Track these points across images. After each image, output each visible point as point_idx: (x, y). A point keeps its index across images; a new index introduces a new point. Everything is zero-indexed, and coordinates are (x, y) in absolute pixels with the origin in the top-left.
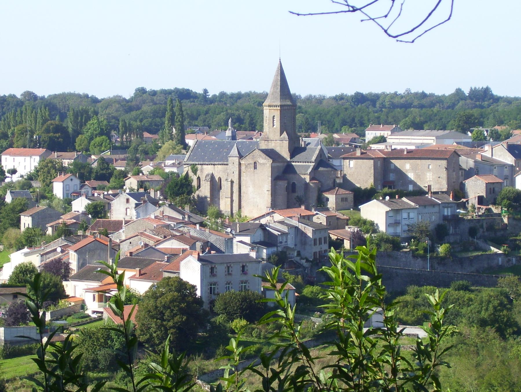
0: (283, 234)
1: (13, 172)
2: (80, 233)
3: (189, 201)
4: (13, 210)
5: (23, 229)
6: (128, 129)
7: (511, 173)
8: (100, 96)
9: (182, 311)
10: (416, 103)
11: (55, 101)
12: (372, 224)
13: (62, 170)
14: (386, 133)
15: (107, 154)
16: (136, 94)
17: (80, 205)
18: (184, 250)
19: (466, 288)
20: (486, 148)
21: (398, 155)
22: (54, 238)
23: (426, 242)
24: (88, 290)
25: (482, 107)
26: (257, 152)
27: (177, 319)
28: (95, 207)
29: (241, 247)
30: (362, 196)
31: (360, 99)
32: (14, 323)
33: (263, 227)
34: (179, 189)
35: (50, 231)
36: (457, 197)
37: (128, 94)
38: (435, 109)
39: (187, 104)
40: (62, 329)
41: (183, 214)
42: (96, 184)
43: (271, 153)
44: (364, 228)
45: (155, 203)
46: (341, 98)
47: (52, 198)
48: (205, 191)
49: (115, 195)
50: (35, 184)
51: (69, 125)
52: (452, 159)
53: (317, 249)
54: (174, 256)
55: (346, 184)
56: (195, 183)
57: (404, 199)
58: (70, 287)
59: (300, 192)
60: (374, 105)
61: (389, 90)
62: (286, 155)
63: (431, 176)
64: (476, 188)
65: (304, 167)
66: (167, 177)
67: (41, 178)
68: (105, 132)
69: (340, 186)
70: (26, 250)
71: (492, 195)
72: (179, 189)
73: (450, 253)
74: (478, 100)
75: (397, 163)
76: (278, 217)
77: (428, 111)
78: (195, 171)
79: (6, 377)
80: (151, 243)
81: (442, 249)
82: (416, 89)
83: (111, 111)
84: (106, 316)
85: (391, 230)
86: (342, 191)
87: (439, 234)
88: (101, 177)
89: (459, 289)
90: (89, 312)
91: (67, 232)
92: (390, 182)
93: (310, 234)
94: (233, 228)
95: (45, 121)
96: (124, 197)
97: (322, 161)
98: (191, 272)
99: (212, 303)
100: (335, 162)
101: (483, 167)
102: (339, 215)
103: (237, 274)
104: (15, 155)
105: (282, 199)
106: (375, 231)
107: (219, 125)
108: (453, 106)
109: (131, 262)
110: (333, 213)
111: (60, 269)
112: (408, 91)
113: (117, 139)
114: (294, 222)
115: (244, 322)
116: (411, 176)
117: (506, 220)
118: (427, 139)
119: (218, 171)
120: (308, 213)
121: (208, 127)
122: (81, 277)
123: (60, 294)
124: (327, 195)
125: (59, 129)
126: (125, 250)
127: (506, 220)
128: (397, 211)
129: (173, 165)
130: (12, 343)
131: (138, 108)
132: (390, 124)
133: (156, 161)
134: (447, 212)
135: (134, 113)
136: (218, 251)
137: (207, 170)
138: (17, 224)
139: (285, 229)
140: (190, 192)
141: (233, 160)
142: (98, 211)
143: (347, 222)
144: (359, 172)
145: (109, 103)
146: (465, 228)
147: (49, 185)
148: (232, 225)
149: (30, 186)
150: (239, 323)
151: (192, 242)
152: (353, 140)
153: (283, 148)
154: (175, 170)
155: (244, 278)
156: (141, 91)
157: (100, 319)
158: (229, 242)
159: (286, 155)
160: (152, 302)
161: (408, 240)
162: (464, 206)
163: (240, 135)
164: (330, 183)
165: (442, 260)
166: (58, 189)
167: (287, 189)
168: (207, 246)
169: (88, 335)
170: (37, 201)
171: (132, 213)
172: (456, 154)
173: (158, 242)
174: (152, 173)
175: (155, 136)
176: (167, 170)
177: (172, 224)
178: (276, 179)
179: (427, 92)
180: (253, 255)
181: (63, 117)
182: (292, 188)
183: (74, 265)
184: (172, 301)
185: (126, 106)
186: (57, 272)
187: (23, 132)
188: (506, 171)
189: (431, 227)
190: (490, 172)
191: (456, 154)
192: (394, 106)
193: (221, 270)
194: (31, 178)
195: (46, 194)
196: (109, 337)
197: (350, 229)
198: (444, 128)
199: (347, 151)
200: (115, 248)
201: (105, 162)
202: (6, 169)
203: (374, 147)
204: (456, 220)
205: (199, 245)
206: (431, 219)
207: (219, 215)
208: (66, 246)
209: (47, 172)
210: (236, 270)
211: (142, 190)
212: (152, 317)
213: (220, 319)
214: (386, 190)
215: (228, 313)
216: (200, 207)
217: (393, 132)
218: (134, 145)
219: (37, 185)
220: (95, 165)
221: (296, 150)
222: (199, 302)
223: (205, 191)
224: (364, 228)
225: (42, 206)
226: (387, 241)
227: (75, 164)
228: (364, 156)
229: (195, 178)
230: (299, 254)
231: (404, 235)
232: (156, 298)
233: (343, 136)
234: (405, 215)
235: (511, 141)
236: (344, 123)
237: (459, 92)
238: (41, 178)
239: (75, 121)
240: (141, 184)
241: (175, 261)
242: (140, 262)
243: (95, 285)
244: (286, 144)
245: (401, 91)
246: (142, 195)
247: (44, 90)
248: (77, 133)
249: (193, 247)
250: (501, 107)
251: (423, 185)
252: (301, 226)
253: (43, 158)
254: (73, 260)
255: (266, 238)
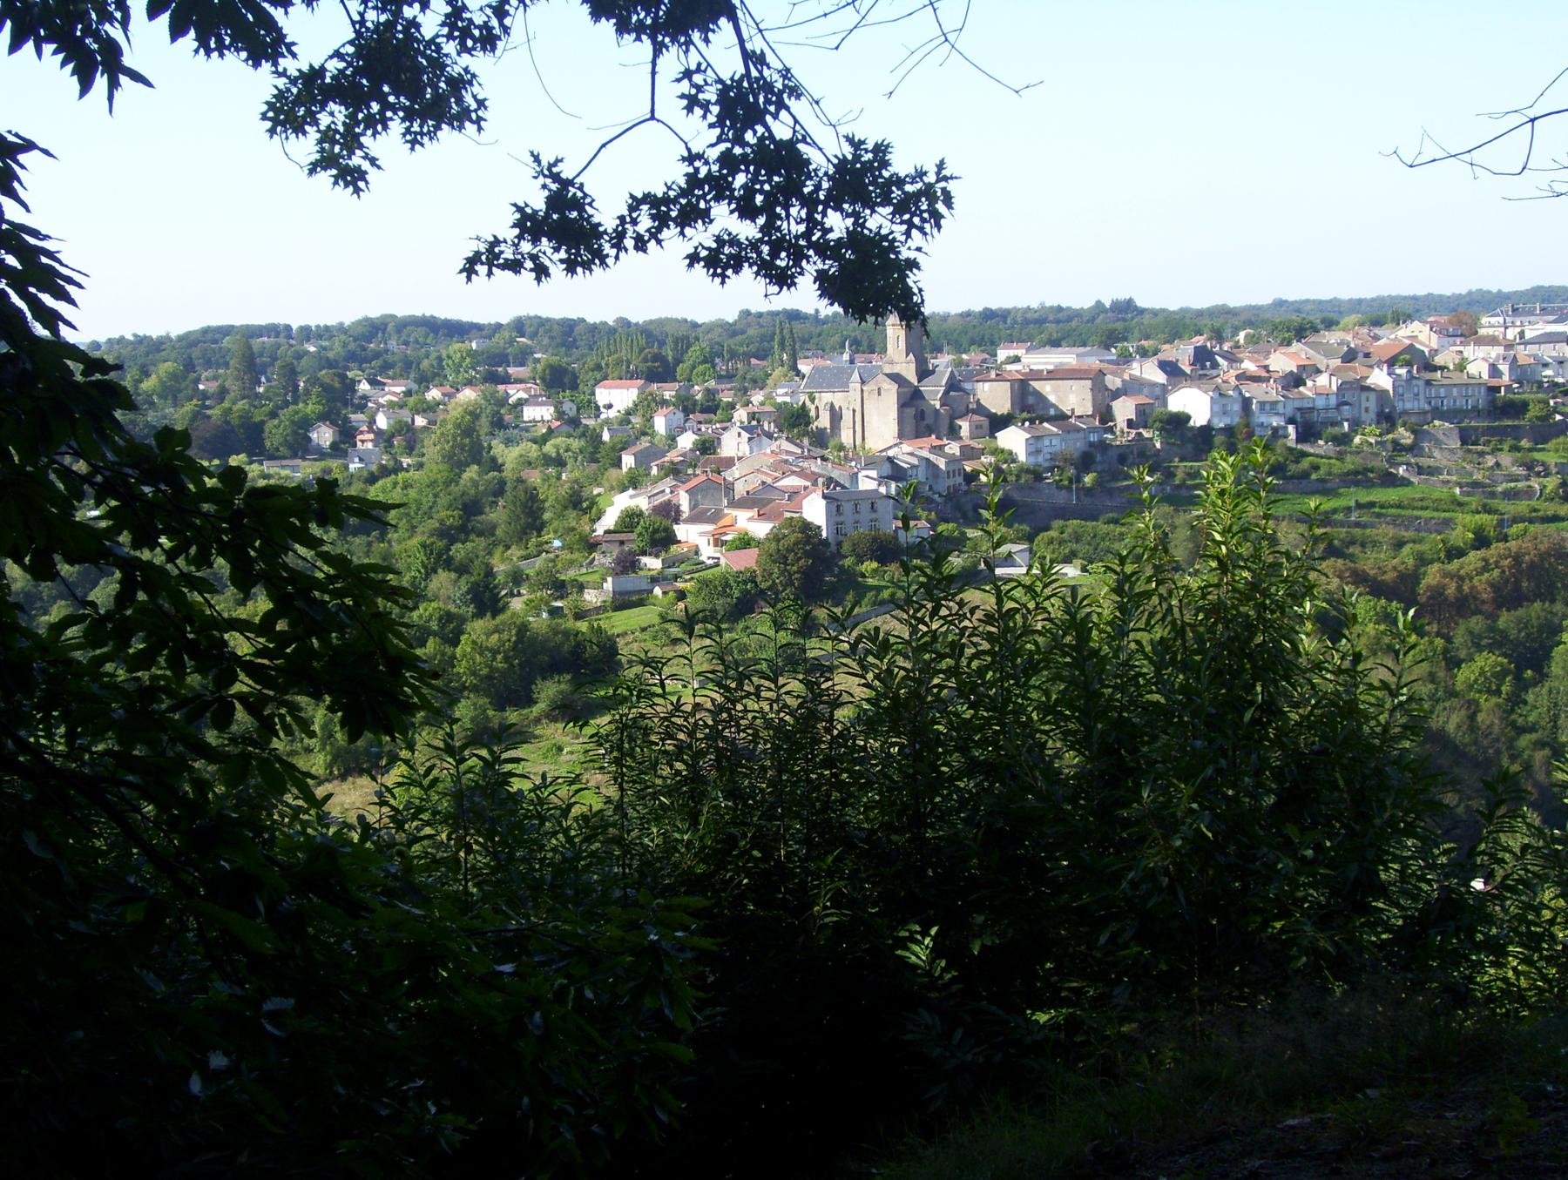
0: (913, 466)
1: (610, 406)
2: (690, 471)
3: (806, 433)
4: (613, 448)
5: (625, 470)
6: (733, 355)
7: (1162, 393)
8: (633, 320)
9: (807, 555)
10: (1051, 318)
11: (652, 327)
12: (1011, 453)
13: (664, 403)
14: (1020, 352)
15: (712, 384)
16: (740, 317)
17: (686, 441)
18: (806, 488)
19: (1115, 522)
20: (1135, 365)
21: (1037, 375)
22: (659, 479)
23: (1072, 471)
24: (702, 534)
25: (1125, 320)
26: (881, 377)
27: (802, 562)
28: (704, 442)
29: (867, 482)
30: (999, 423)
31: (988, 314)
32: (622, 573)
33: (890, 460)
34: (795, 421)
35: (654, 471)
36: (1103, 421)
37: (731, 317)
38: (1074, 324)
39: (797, 326)
40: (676, 577)
41: (802, 448)
42: (701, 417)
43: (896, 378)
44: (1001, 457)
45: (770, 436)
46: (968, 314)
47: (653, 435)
48: (824, 422)
49: (724, 429)
50: (634, 420)
51: (670, 355)
52: (1097, 378)
53: (951, 482)
54: (794, 494)
55: (980, 410)
56: (813, 414)
57: (1045, 425)
58: (681, 531)
59: (929, 420)
60: (1005, 322)
61: (1022, 304)
62: (913, 379)
63: (1074, 399)
64: (1124, 410)
65: (933, 392)
66: (780, 407)
67: (640, 412)
68: (709, 360)
69: (974, 412)
70: (631, 492)
71: (1142, 418)
72: (795, 421)
73: (1098, 483)
74: (1120, 312)
75: (1036, 385)
76: (906, 448)
77: (1067, 327)
78: (813, 400)
79: (616, 631)
80: (769, 481)
81: (1088, 479)
82: (1051, 302)
83: (714, 336)
84: (723, 561)
85: (1032, 459)
86: (976, 417)
87: (1085, 462)
88: (704, 410)
89: (1108, 522)
90: (703, 558)
91: (675, 471)
92: (1029, 406)
93: (943, 467)
94: (858, 460)
95: (641, 350)
96: (735, 430)
97: (953, 385)
98: (815, 511)
99: (839, 544)
100: (967, 386)
101: (1132, 387)
102: (974, 444)
103: (865, 513)
104: (610, 387)
105: (909, 428)
106: (1014, 461)
107: (833, 349)
108: (1093, 320)
109: (746, 503)
110: (967, 442)
111: (669, 512)
112: (1042, 305)
113: (721, 367)
114: (925, 454)
115: (875, 565)
116: (1052, 398)
117: (1158, 445)
118: (1066, 357)
119: (838, 399)
120: (940, 443)
121: (822, 351)
122: (693, 519)
123: (670, 539)
124: (959, 422)
125: (657, 357)
126: (740, 489)
127: (1158, 445)
128: (1038, 438)
129: (786, 394)
130: (621, 593)
131: (743, 332)
132: (1024, 341)
133: (767, 390)
134: (1093, 438)
135: (739, 338)
136: (843, 487)
137: (825, 398)
138: (618, 463)
139: (915, 461)
140: (808, 424)
141: (855, 385)
142: (707, 447)
143: (982, 452)
144: (995, 396)
145: (711, 327)
146: (1113, 454)
147: (649, 420)
148: (856, 458)
149: (629, 422)
150: (869, 566)
151: (813, 478)
152: (984, 361)
153: (910, 374)
154: (788, 399)
155: (874, 516)
156: (746, 314)
157: (717, 565)
158: (854, 477)
159: (913, 379)
160: (773, 546)
161: (1051, 469)
162: (1111, 430)
163: (859, 358)
164: (963, 408)
165: (1089, 491)
166: (660, 424)
167: (916, 418)
168: (830, 481)
169: (705, 583)
170: (637, 438)
171: (745, 448)
172: (1102, 373)
173: (777, 479)
174: (762, 404)
175: (764, 363)
176: (779, 400)
177: (791, 459)
178: (903, 406)
179: (1064, 305)
180: (883, 490)
181: (662, 343)
182: (921, 415)
183: (685, 507)
184: (796, 544)
185: (731, 330)
186: (667, 516)
187: (619, 362)
188: (1158, 391)
189: (1076, 455)
190: (1140, 392)
191: (1102, 373)
192: (1027, 322)
193: (847, 508)
194: (628, 413)
195: (647, 431)
196: (727, 585)
197: (987, 459)
198: (1084, 345)
199: (979, 373)
200: (729, 488)
201: (710, 393)
202: (601, 404)
203: (1009, 367)
204: (1103, 446)
205: (820, 481)
206: (1076, 446)
207: (841, 448)
208: (675, 486)
209: (647, 405)
210: (865, 507)
211: (754, 423)
212: (774, 562)
213: (848, 562)
214: (1025, 415)
215: (857, 556)
216: (820, 439)
217: (1028, 350)
218: (741, 373)
219: (636, 420)
220: (699, 397)
221: (924, 373)
222: (825, 543)
223: (824, 422)
224: (1001, 457)
225: (644, 443)
226: (1028, 471)
227: (677, 396)
228: (1000, 378)
229: (813, 407)
230: (931, 488)
231: (1047, 464)
232: (779, 541)
233: (972, 357)
234: (1047, 442)
235: (1161, 356)
236: (972, 342)
237: (1099, 303)
238: (640, 412)
239: (675, 349)
240: (752, 416)
241: (798, 498)
242: (757, 501)
243: (710, 527)
244: (913, 366)
245: (1035, 305)
246: (755, 427)
247: (638, 316)
248: (678, 361)
249: (815, 484)
250: (1146, 319)
251: (1066, 409)
252: (932, 457)
253: (642, 390)
254: (684, 501)
255: (896, 472)
